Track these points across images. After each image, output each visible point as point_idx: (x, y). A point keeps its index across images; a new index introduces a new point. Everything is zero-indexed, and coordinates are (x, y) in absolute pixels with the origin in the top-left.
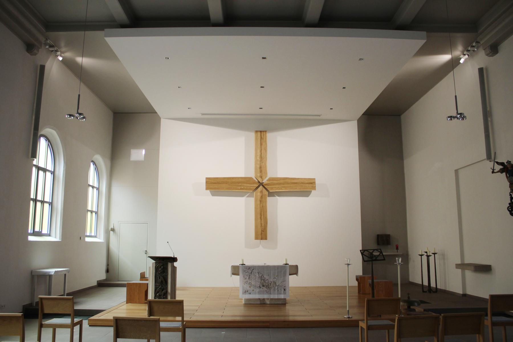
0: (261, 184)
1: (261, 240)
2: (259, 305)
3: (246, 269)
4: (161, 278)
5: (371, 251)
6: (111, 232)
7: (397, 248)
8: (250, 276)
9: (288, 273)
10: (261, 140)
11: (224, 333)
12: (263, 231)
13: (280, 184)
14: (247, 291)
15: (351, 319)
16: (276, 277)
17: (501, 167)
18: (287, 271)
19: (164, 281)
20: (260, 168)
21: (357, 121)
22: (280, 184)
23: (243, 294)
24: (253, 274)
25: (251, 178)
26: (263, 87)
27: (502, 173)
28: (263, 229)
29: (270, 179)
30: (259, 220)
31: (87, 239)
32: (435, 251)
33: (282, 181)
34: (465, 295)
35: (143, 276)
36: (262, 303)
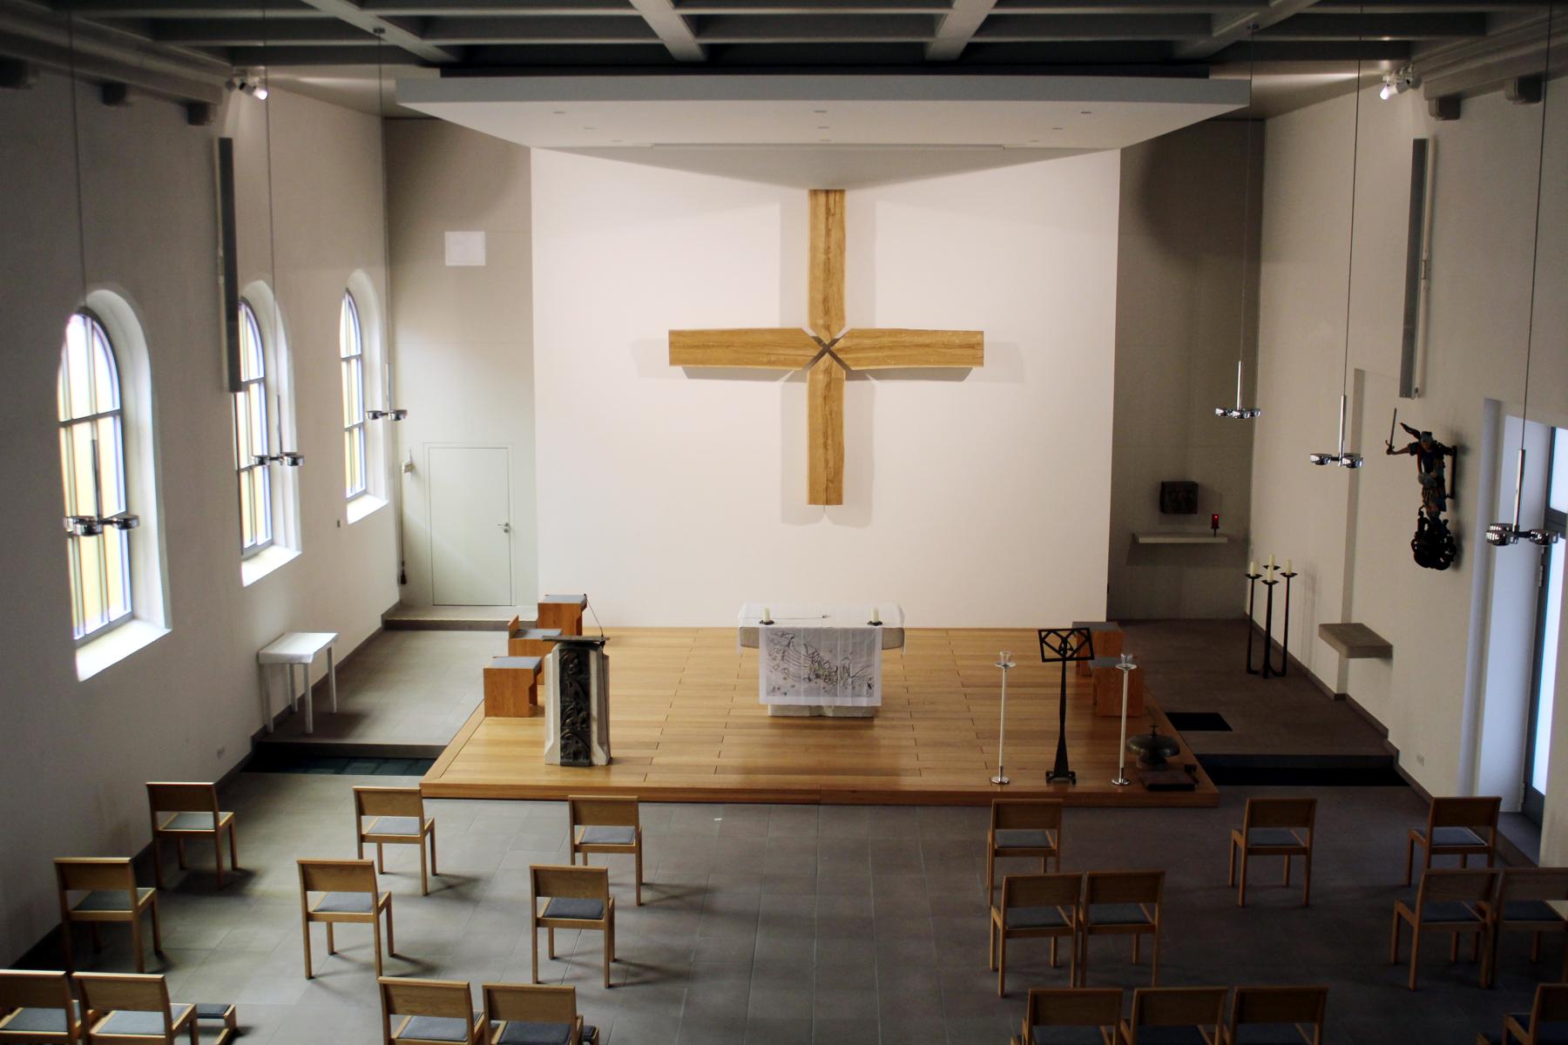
1: (827, 506)
2: (807, 722)
3: (775, 637)
4: (575, 684)
5: (1064, 634)
6: (407, 477)
7: (1215, 525)
8: (784, 653)
10: (827, 219)
11: (720, 819)
12: (832, 482)
14: (779, 689)
15: (1005, 789)
16: (850, 658)
17: (1414, 440)
18: (876, 640)
20: (825, 300)
23: (768, 694)
24: (792, 648)
25: (799, 332)
27: (1412, 454)
28: (833, 475)
30: (821, 451)
32: (1290, 569)
33: (886, 340)
34: (1342, 698)
36: (816, 714)
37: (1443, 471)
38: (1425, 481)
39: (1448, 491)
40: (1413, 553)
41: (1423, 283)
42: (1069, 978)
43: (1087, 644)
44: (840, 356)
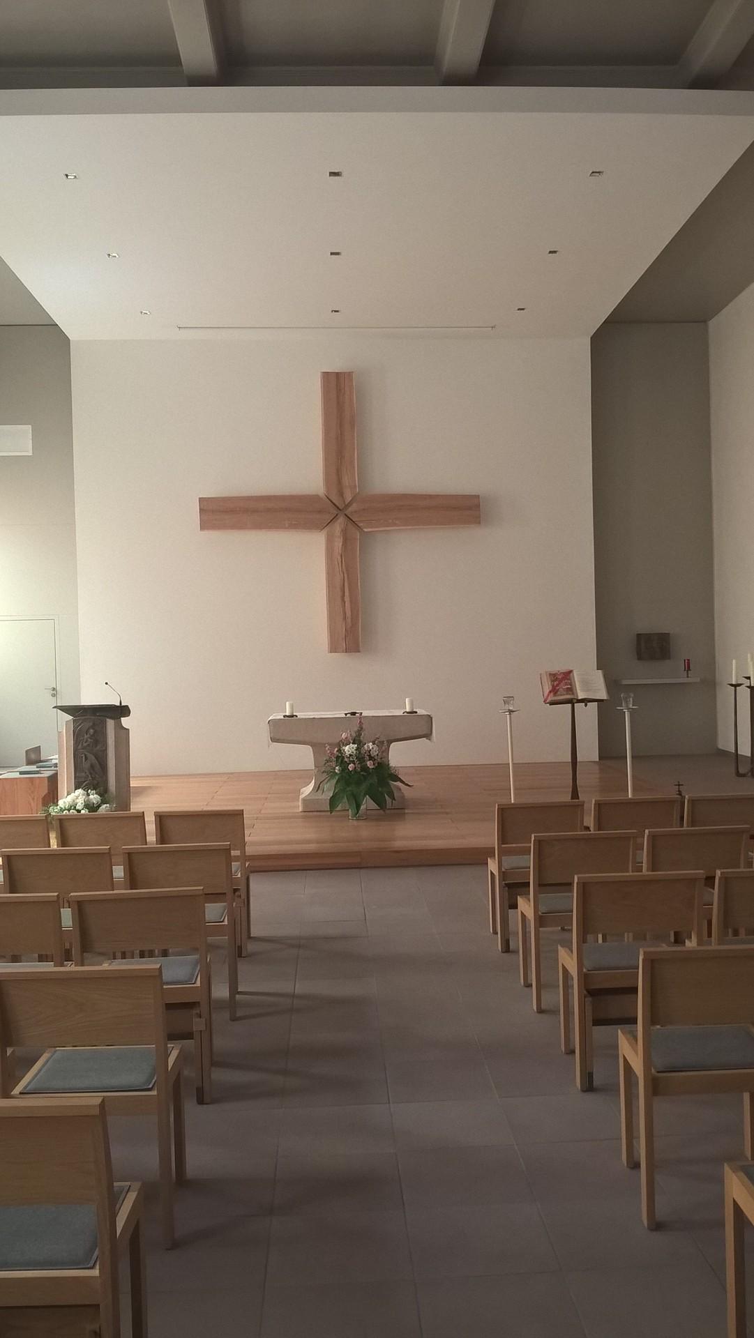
7: (688, 668)
19: (98, 766)
26: (338, 254)
35: (34, 757)
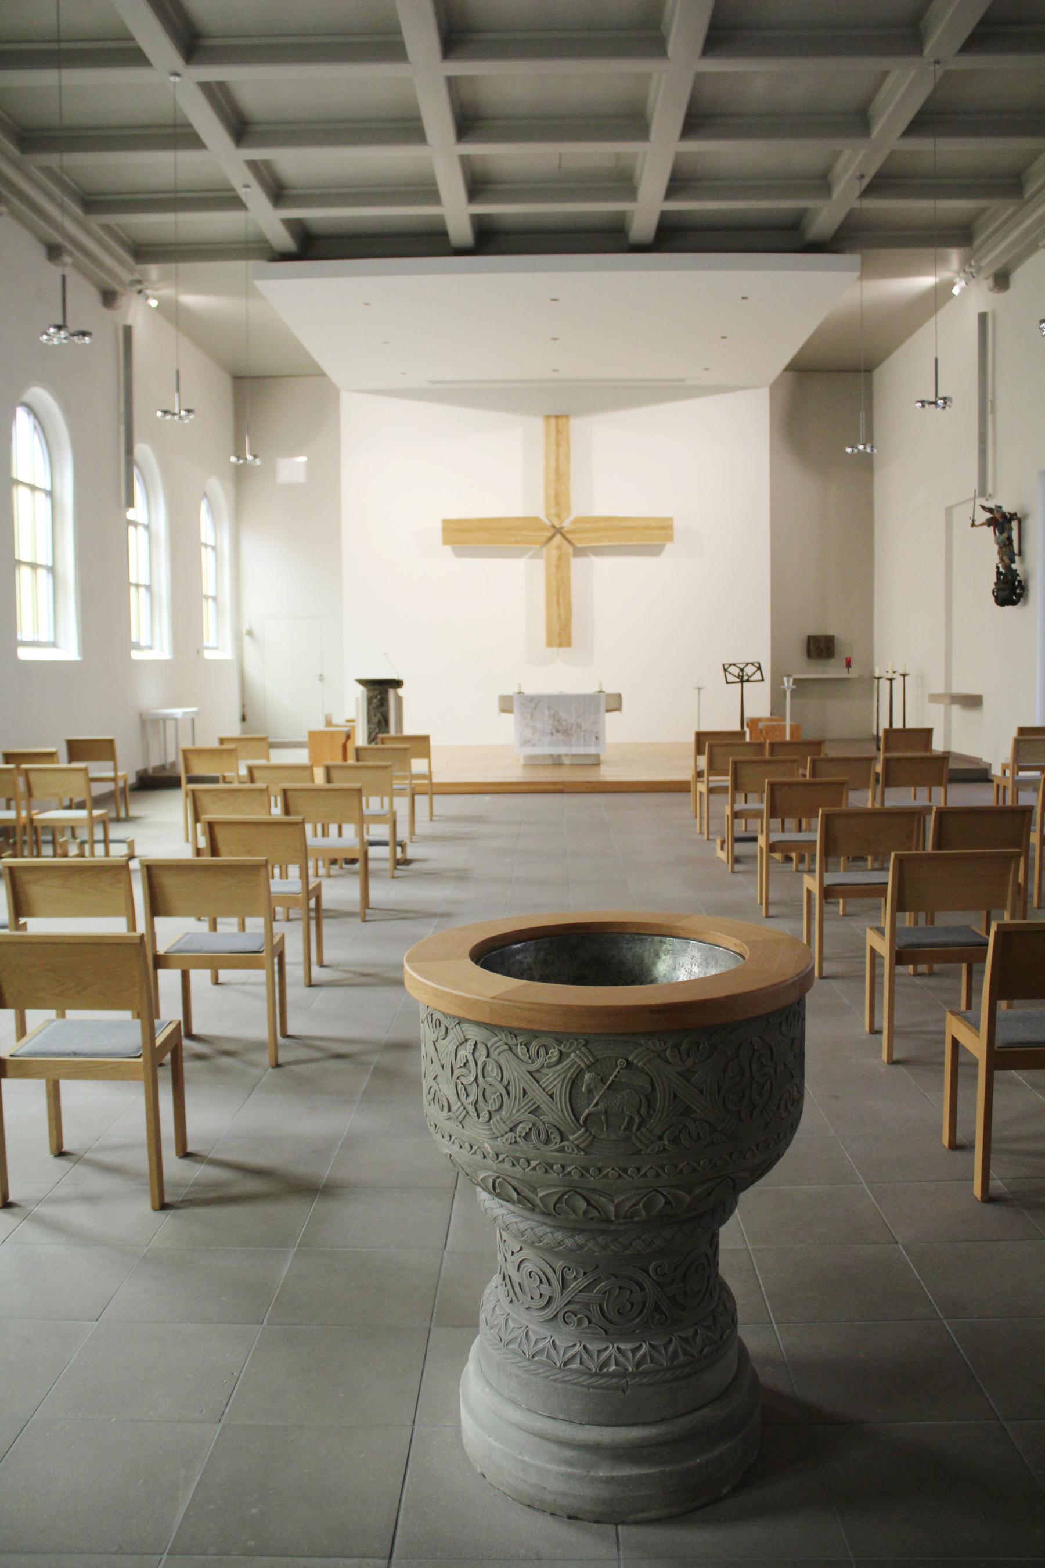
0: (558, 531)
5: (742, 666)
6: (247, 639)
7: (848, 664)
9: (603, 708)
13: (598, 530)
17: (989, 515)
20: (557, 495)
21: (765, 392)
22: (598, 530)
25: (536, 519)
27: (989, 526)
29: (578, 520)
31: (24, 654)
37: (1011, 533)
38: (1000, 541)
39: (1016, 551)
40: (995, 580)
41: (990, 417)
42: (756, 873)
43: (759, 672)
44: (569, 536)
